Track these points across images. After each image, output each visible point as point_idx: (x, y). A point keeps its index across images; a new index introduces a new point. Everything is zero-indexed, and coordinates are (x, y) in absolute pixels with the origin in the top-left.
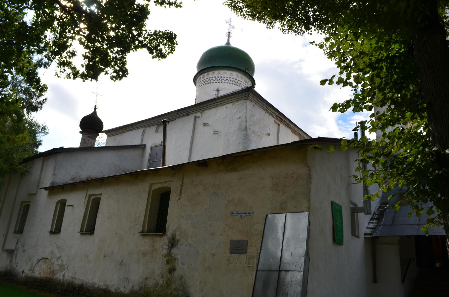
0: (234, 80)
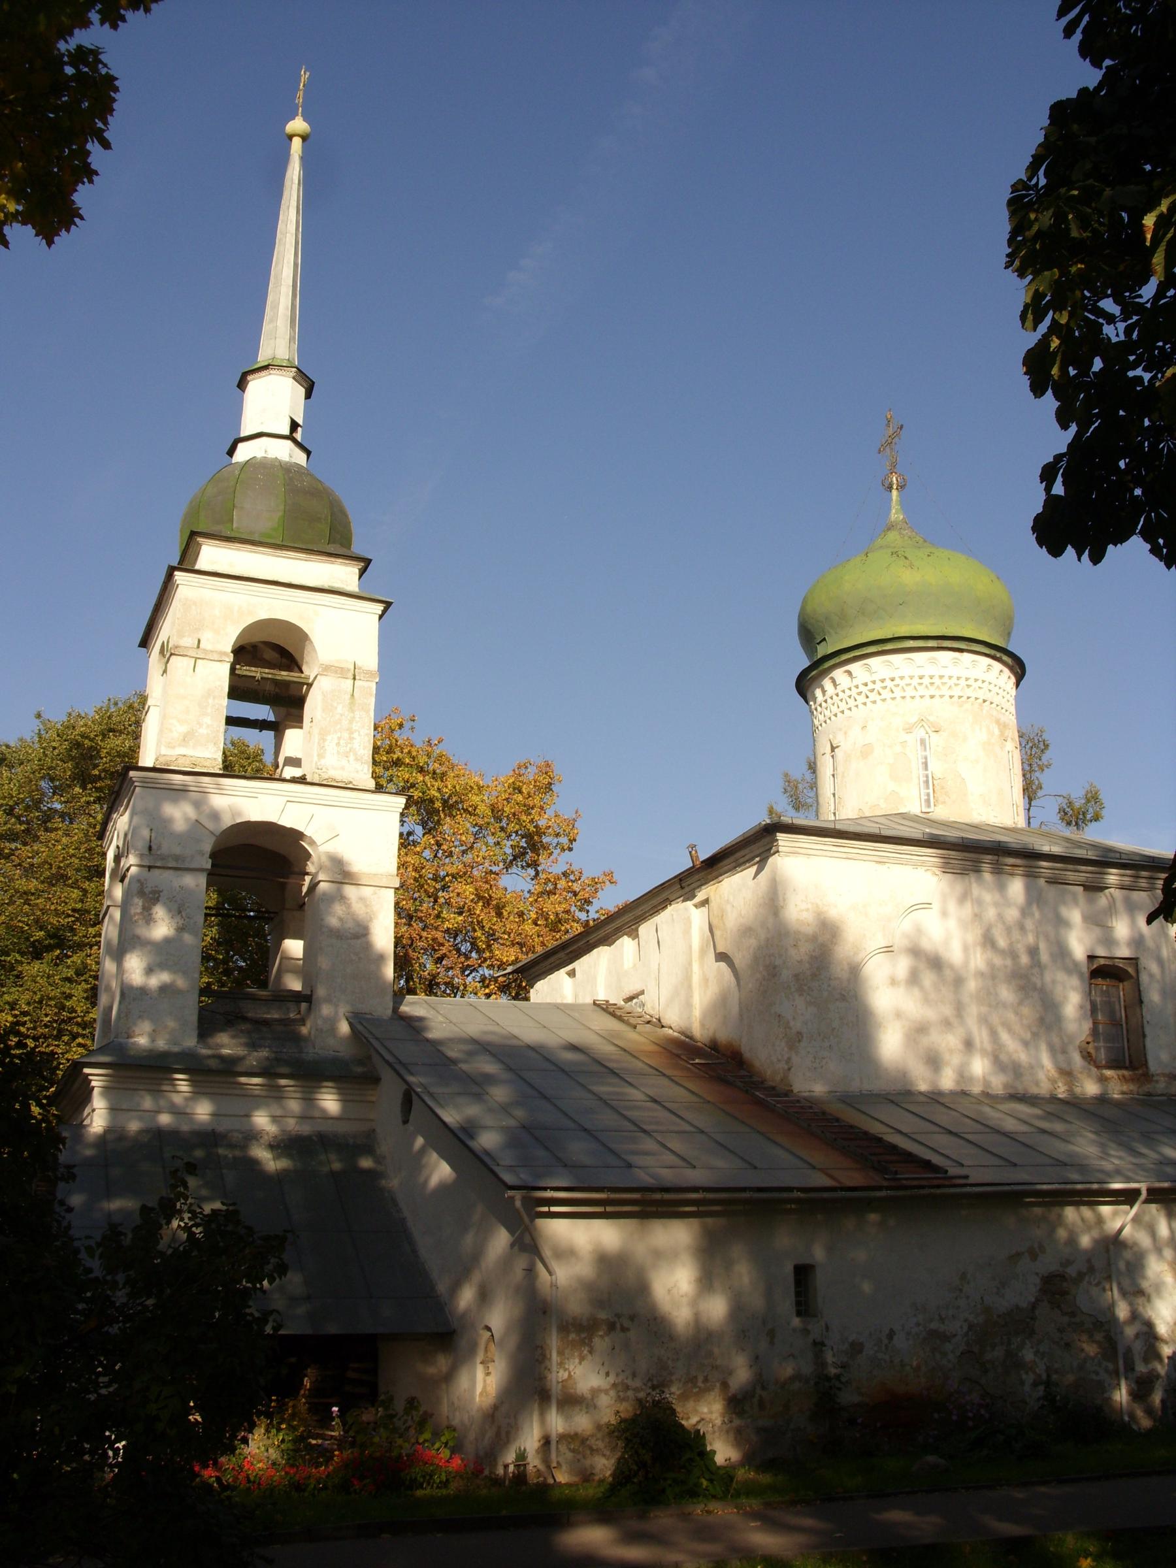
0: (907, 680)
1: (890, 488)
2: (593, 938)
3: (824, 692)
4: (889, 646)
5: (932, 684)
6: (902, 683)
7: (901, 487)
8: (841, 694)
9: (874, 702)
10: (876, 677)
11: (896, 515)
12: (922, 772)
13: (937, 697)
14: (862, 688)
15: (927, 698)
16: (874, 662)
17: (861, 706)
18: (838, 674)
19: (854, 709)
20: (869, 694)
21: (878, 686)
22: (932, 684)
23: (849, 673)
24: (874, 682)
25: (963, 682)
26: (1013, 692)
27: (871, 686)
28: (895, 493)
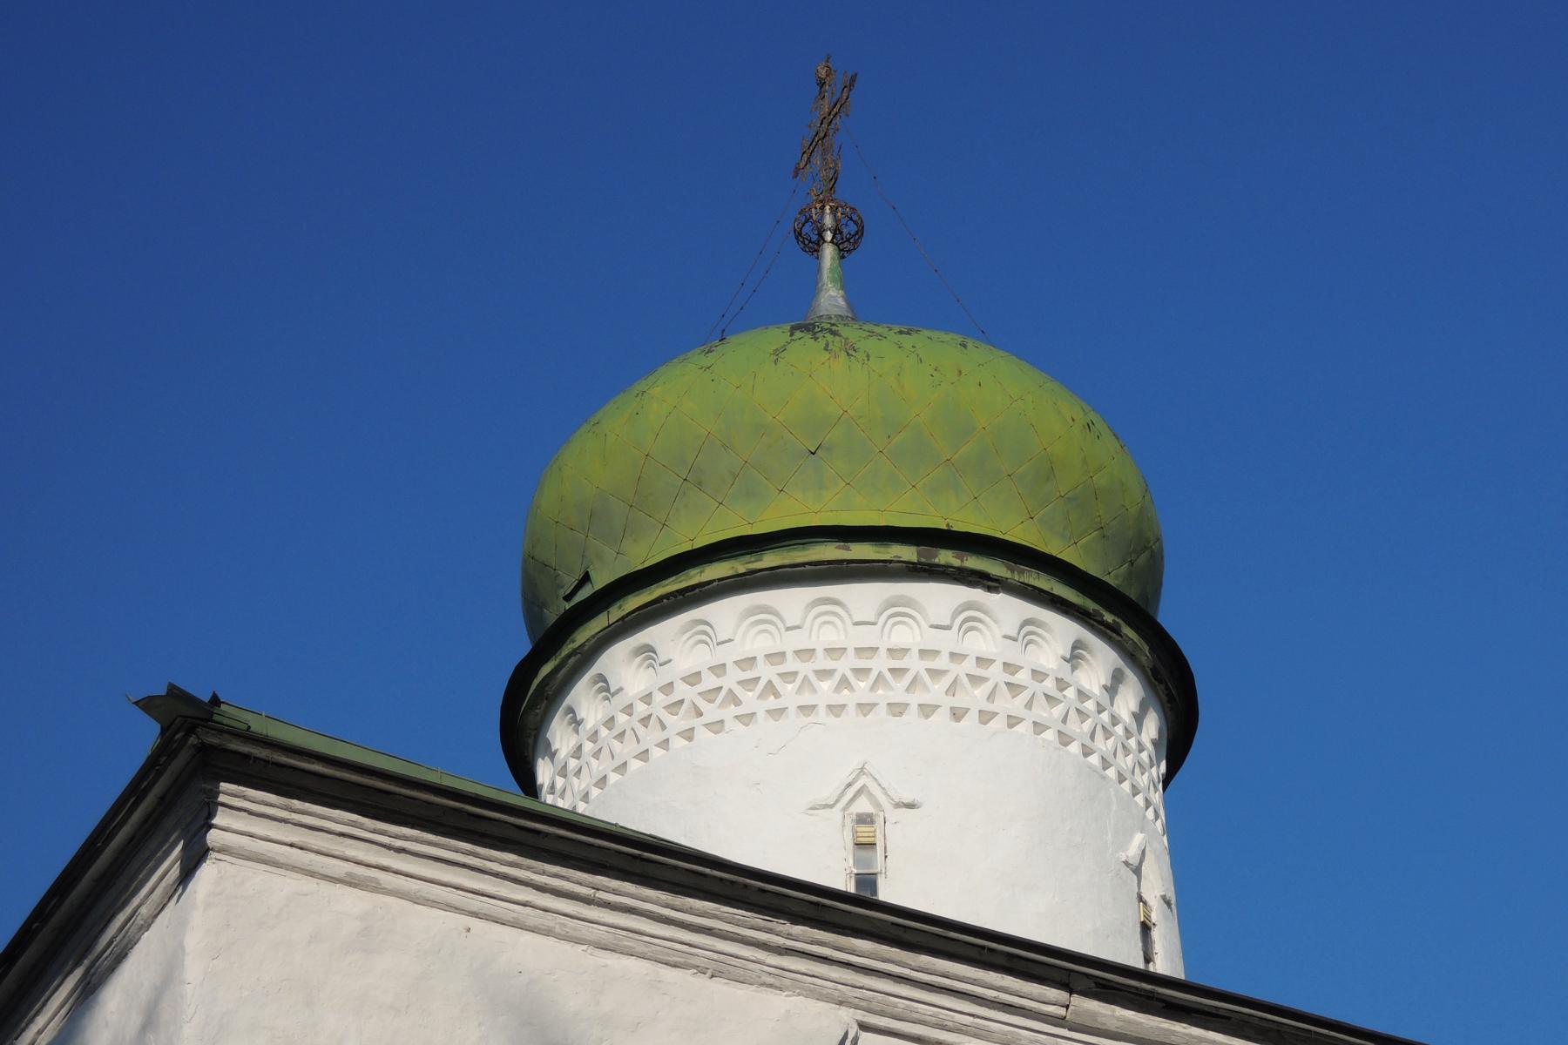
1: (814, 247)
2: (94, 980)
3: (576, 723)
4: (770, 559)
5: (897, 672)
6: (805, 668)
7: (847, 244)
8: (622, 718)
9: (717, 726)
10: (727, 655)
11: (831, 298)
12: (851, 646)
13: (913, 713)
14: (682, 690)
15: (882, 709)
16: (724, 613)
17: (678, 743)
18: (617, 661)
19: (656, 753)
20: (702, 704)
21: (730, 680)
22: (897, 672)
23: (647, 650)
24: (719, 670)
25: (995, 673)
26: (1157, 797)
27: (709, 682)
28: (829, 252)
